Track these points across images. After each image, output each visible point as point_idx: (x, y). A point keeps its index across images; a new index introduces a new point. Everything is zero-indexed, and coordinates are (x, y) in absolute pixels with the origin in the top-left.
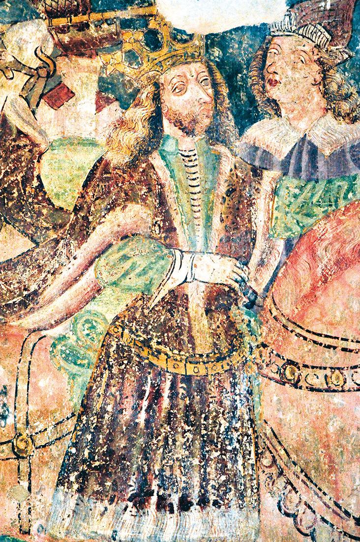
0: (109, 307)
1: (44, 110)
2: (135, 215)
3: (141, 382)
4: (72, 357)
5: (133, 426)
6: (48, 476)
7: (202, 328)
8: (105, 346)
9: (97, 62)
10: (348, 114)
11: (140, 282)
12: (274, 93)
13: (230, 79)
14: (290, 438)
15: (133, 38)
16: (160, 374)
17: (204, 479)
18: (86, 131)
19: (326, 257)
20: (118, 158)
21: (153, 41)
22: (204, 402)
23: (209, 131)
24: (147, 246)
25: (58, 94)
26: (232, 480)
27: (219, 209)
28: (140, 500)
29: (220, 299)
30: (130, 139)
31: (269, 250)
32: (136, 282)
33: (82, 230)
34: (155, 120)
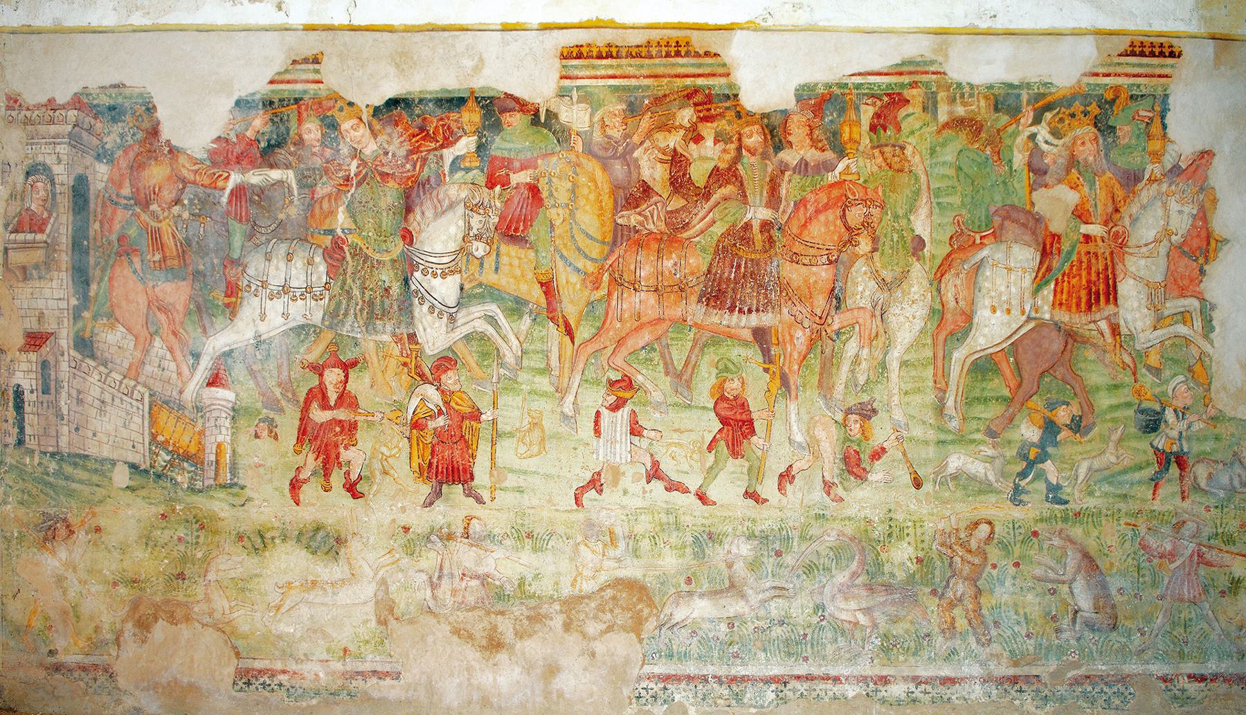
0: (719, 229)
1: (692, 146)
2: (728, 190)
3: (732, 261)
4: (704, 250)
5: (729, 279)
6: (694, 298)
7: (759, 238)
8: (717, 246)
9: (715, 125)
10: (890, 535)
11: (733, 219)
12: (790, 138)
13: (771, 132)
14: (794, 285)
15: (730, 114)
16: (741, 258)
17: (758, 301)
18: (710, 154)
19: (811, 209)
20: (722, 166)
21: (739, 115)
22: (759, 270)
23: (762, 154)
24: (735, 203)
25: (698, 139)
26: (770, 301)
27: (766, 187)
28: (732, 309)
29: (766, 226)
30: (728, 157)
31: (787, 206)
32: (730, 219)
33: (707, 196)
34: (739, 149)
